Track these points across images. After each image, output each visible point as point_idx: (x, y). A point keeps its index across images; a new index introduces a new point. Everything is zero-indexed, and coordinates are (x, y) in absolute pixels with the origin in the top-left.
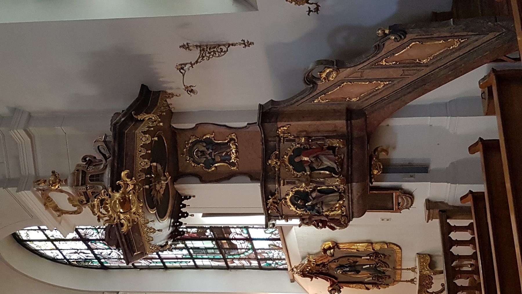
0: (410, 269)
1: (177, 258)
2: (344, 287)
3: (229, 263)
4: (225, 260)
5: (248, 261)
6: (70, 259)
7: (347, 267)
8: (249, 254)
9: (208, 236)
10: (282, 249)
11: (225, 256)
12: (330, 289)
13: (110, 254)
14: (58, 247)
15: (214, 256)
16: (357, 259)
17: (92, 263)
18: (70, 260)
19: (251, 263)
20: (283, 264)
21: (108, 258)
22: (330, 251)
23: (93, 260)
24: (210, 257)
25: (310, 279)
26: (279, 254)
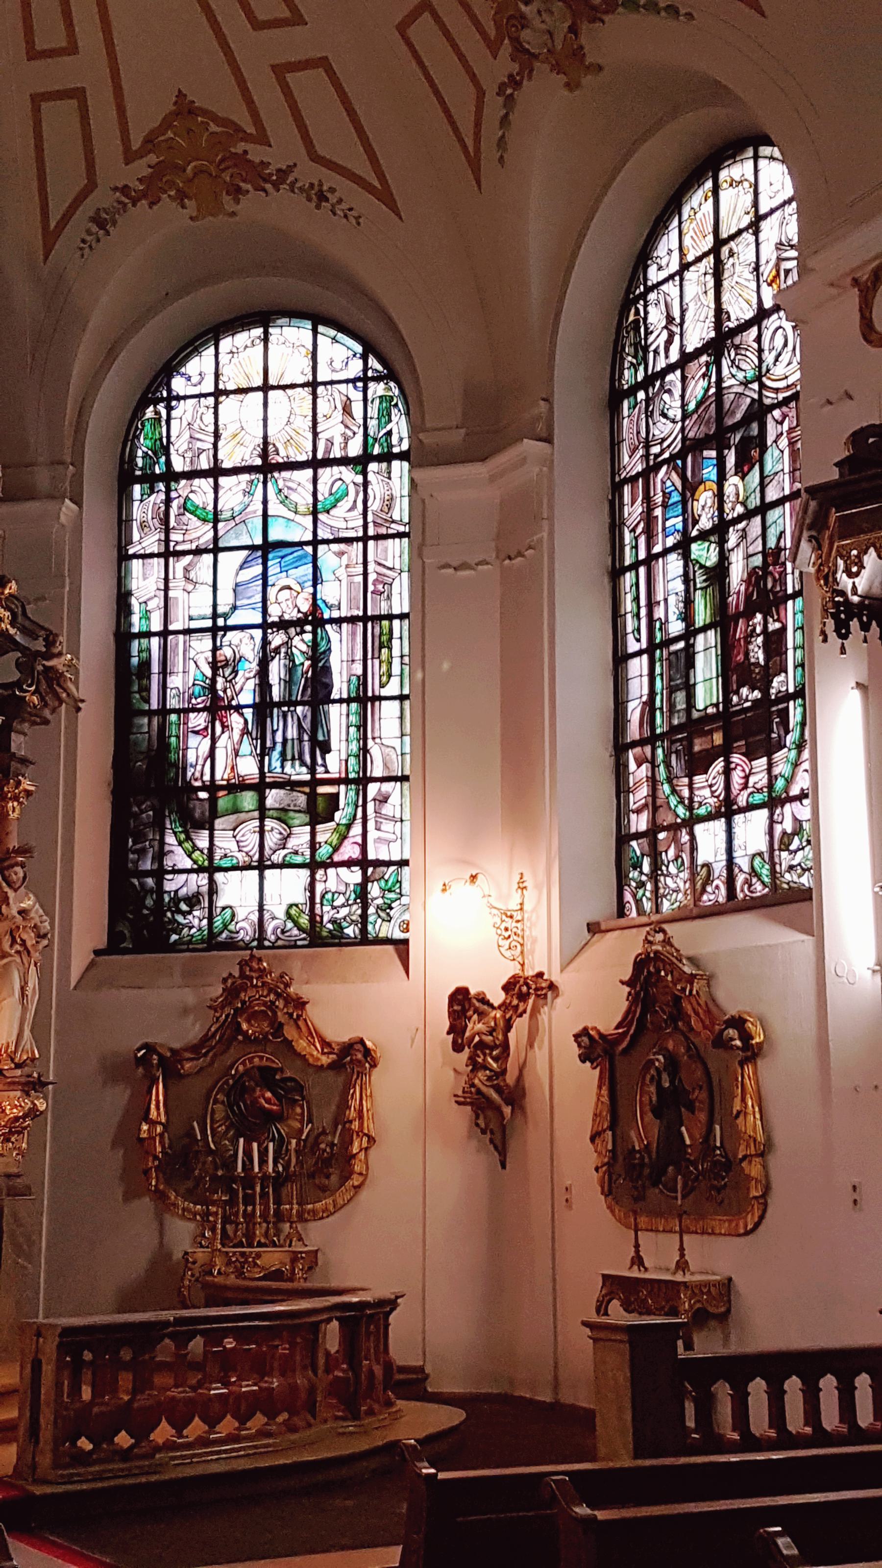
0: (682, 1255)
1: (651, 605)
2: (598, 1069)
3: (638, 750)
4: (651, 740)
5: (646, 805)
6: (646, 302)
7: (672, 1082)
8: (673, 807)
9: (737, 692)
10: (697, 899)
11: (663, 742)
12: (592, 1033)
13: (665, 416)
14: (692, 268)
15: (661, 709)
16: (701, 1110)
17: (632, 363)
18: (642, 302)
19: (638, 811)
20: (638, 902)
21: (652, 412)
22: (736, 1036)
23: (642, 368)
24: (658, 698)
25: (626, 978)
26: (674, 891)
